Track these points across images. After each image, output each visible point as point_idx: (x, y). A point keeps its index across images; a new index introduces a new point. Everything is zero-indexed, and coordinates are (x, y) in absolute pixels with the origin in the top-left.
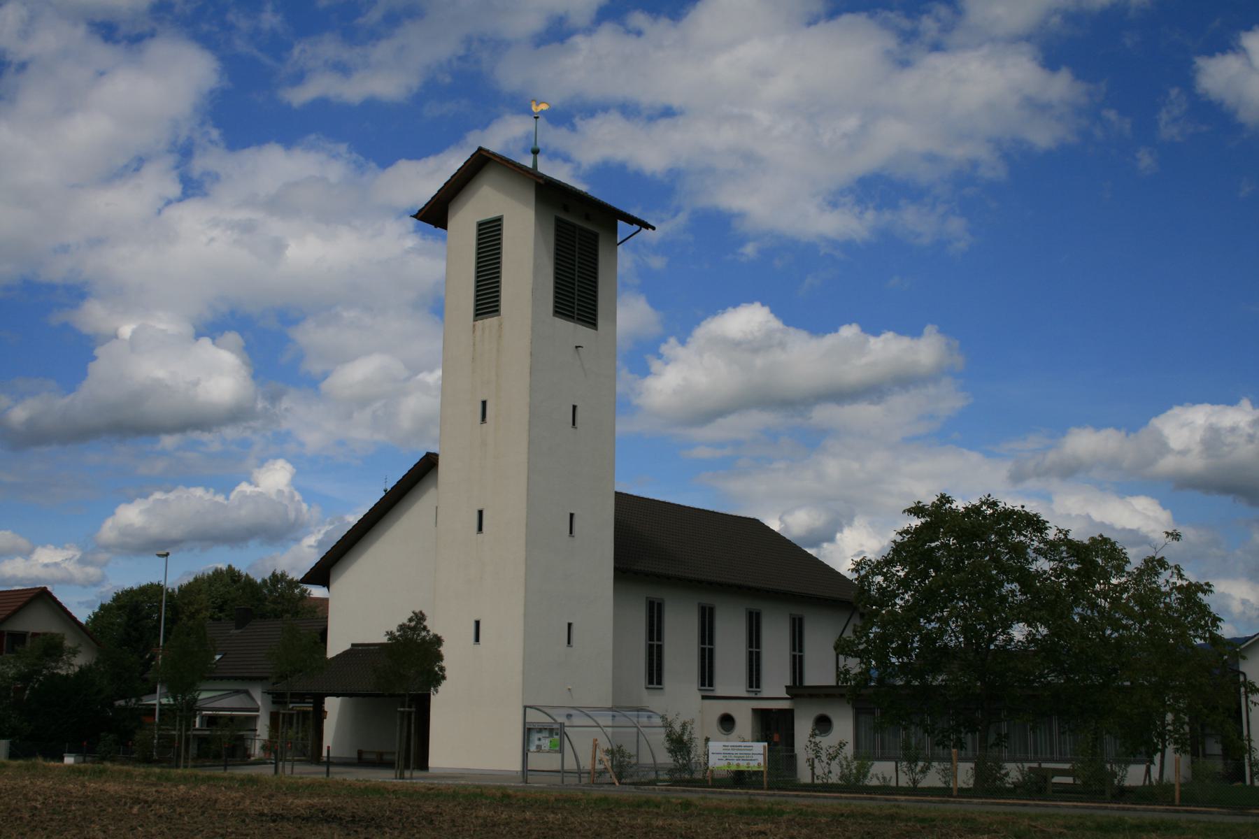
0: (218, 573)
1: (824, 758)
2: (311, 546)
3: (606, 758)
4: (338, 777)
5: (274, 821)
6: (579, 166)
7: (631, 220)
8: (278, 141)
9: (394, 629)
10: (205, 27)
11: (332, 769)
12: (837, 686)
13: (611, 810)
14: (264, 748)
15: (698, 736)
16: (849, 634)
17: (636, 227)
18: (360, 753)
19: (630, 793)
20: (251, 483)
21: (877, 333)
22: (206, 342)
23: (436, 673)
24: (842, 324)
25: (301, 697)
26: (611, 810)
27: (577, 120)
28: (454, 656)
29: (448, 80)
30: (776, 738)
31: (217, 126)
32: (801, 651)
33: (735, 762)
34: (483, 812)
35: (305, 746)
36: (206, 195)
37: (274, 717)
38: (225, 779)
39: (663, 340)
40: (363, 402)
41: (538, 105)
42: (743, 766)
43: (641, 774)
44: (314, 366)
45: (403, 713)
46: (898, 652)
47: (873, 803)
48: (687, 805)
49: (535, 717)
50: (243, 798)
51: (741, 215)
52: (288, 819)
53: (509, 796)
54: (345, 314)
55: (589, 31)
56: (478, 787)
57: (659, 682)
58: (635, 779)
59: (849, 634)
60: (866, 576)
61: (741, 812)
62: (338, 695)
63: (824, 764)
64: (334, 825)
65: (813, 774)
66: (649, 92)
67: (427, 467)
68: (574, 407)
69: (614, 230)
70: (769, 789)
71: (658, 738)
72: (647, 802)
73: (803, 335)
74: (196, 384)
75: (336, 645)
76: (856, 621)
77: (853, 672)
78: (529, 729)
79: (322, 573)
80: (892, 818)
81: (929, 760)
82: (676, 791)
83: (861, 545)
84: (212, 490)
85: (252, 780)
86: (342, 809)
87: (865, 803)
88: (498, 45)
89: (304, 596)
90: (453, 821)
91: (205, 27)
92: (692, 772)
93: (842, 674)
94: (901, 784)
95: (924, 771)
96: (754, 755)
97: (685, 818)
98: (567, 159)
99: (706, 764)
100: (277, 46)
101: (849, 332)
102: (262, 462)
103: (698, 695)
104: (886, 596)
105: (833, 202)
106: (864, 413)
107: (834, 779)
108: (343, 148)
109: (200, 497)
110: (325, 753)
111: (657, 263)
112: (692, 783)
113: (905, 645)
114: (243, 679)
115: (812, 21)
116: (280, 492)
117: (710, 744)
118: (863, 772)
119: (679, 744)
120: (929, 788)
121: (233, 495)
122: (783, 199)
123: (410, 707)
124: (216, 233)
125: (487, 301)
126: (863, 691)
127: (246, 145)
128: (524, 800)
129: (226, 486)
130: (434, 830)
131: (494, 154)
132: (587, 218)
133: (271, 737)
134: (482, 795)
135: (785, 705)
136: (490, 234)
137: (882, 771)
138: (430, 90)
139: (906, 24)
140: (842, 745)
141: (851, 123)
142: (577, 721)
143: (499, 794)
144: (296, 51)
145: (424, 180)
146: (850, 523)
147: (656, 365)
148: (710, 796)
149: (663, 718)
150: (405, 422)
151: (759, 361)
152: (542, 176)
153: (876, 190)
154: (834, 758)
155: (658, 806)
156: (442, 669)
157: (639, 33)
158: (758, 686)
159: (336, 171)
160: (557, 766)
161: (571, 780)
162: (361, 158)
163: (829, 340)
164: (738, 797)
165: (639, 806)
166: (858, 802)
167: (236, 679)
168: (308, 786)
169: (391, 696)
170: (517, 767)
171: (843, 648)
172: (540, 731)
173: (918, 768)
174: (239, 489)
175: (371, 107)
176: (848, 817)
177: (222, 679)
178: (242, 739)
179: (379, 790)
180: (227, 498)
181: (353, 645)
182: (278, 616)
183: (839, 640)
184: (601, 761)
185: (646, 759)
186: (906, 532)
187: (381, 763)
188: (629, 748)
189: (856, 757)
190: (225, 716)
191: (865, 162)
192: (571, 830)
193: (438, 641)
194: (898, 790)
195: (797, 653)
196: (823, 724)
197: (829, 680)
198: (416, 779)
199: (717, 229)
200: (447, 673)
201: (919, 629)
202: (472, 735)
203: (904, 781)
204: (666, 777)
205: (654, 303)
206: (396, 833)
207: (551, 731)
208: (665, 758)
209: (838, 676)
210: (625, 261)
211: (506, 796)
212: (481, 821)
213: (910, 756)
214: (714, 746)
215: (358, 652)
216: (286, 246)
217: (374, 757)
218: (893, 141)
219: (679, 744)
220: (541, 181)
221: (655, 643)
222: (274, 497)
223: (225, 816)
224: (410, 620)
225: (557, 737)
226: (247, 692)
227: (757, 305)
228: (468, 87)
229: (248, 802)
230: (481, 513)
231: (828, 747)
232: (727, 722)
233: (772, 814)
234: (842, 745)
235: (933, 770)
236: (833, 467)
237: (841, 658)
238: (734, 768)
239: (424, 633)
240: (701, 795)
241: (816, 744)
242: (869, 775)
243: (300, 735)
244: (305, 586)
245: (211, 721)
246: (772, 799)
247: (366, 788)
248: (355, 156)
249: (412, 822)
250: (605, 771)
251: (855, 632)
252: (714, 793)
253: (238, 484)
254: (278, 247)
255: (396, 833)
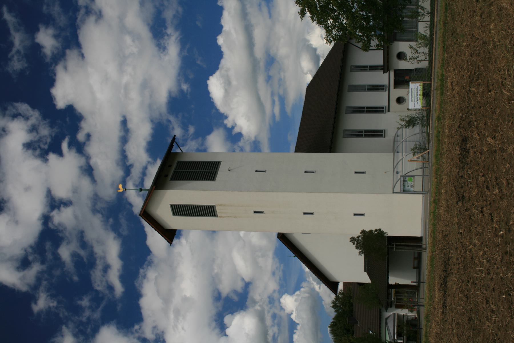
0: (332, 332)
1: (417, 55)
2: (320, 288)
3: (416, 156)
4: (426, 278)
5: (446, 307)
6: (149, 162)
7: (171, 146)
8: (139, 300)
9: (358, 251)
10: (89, 330)
11: (422, 281)
12: (384, 50)
13: (441, 154)
14: (412, 311)
15: (406, 113)
16: (360, 45)
17: (174, 144)
18: (414, 268)
19: (433, 145)
20: (292, 313)
21: (222, 27)
22: (228, 331)
23: (378, 233)
24: (217, 44)
25: (389, 295)
26: (441, 154)
27: (128, 164)
28: (370, 226)
29: (111, 220)
30: (407, 78)
31: (133, 326)
32: (367, 67)
33: (419, 96)
34: (442, 212)
35: (411, 293)
36: (163, 332)
37: (398, 307)
38: (426, 329)
39: (225, 126)
40: (255, 263)
41: (119, 189)
42: (420, 93)
43: (424, 140)
44: (239, 286)
45: (396, 248)
46: (368, 22)
47: (438, 32)
48: (439, 119)
49: (398, 188)
50: (435, 321)
51: (170, 93)
52: (445, 300)
53: (434, 200)
54: (216, 271)
55: (88, 158)
56: (430, 214)
57: (382, 131)
58: (426, 142)
59: (360, 45)
60: (333, 37)
61: (442, 94)
62: (388, 278)
63: (420, 55)
64: (448, 280)
65: (424, 60)
66: (114, 133)
67: (283, 237)
68: (256, 171)
69: (176, 154)
70: (431, 81)
71: (407, 132)
72: (437, 137)
73: (223, 62)
74: (248, 335)
75: (365, 279)
76: (354, 41)
77: (378, 43)
78: (404, 191)
79: (332, 285)
80: (445, 24)
81: (418, 6)
82: (432, 123)
83: (318, 36)
84: (295, 331)
85: (427, 317)
86: (440, 276)
87: (438, 36)
88: (96, 198)
89: (342, 294)
90: (446, 225)
91: (89, 330)
92: (423, 116)
93: (378, 48)
94: (429, 20)
95: (423, 9)
96: (415, 88)
97: (445, 119)
98: (146, 168)
99: (419, 110)
100: (98, 299)
101: (221, 40)
102: (282, 309)
103: (387, 113)
104: (342, 27)
105: (162, 48)
106: (259, 34)
107: (426, 50)
108: (141, 271)
109: (298, 336)
110: (414, 284)
111: (192, 130)
112: (428, 116)
113: (363, 19)
114: (380, 321)
115: (83, 56)
116: (296, 300)
117: (410, 108)
118: (424, 37)
119: (410, 122)
120: (431, 6)
121: (297, 321)
122: (161, 73)
123: (393, 245)
124: (180, 327)
125: (209, 211)
126: (386, 38)
127: (141, 313)
128: (436, 193)
129: (293, 326)
130: (450, 234)
131: (142, 209)
132: (170, 166)
133: (407, 308)
134: (434, 212)
135: (392, 74)
136: (179, 210)
137: (423, 28)
138: (115, 228)
139: (82, 11)
140: (411, 47)
141: (128, 39)
142: (400, 169)
143: (433, 205)
144: (99, 288)
145: (155, 240)
146: (308, 41)
147: (236, 130)
148: (434, 108)
149: (399, 129)
150: (264, 242)
151: (234, 83)
152: (152, 187)
153: (157, 30)
154: (417, 51)
155: (439, 132)
156: (376, 230)
157: (89, 136)
158: (384, 86)
159: (151, 274)
160: (420, 178)
161: (427, 171)
162: (146, 263)
163: (224, 49)
164: (435, 95)
165: (439, 140)
166: (438, 40)
167: (380, 324)
168: (430, 291)
169: (388, 254)
170: (420, 197)
171: (366, 48)
172: (404, 186)
173: (422, 11)
174: (294, 319)
175: (123, 256)
176: (444, 44)
177: (380, 330)
178: (407, 321)
179: (432, 259)
180: (299, 324)
181: (365, 271)
182: (351, 305)
183: (363, 49)
184: (418, 158)
185: (418, 137)
186: (312, 19)
187: (419, 258)
188: (412, 145)
189: (417, 41)
190: (397, 329)
191: (145, 33)
192: (450, 172)
193: (363, 232)
194: (432, 21)
195: (368, 68)
196: (401, 56)
197: (381, 53)
198: (427, 243)
199: (176, 103)
200: (378, 228)
201: (357, 11)
202: (405, 216)
203: (428, 18)
204: (425, 128)
205: (209, 131)
206: (452, 251)
207: (404, 181)
208: (417, 129)
209: (379, 49)
210: (190, 152)
211: (434, 201)
212: (446, 213)
213: (416, 15)
214: (411, 106)
215: (368, 268)
216: (185, 296)
217: (416, 262)
218: (136, 20)
219: (410, 122)
220: (154, 187)
221: (364, 133)
222: (298, 303)
223: (443, 329)
224: (354, 244)
225: (407, 178)
226: (387, 319)
227: (209, 82)
228: (114, 211)
229: (437, 319)
230: (305, 213)
231: (411, 53)
232: (400, 100)
233: (443, 79)
234: (411, 47)
235: (423, 5)
236: (283, 50)
237: (371, 48)
238: (421, 97)
239: (360, 238)
240: (434, 112)
241: (410, 59)
242: (425, 34)
243: (406, 295)
244: (338, 293)
245: (400, 335)
246: (436, 79)
247: (431, 265)
248: (145, 266)
249: (446, 244)
250: (423, 156)
251: (359, 42)
252: (433, 106)
253: (292, 319)
254: (185, 299)
255: (452, 251)
